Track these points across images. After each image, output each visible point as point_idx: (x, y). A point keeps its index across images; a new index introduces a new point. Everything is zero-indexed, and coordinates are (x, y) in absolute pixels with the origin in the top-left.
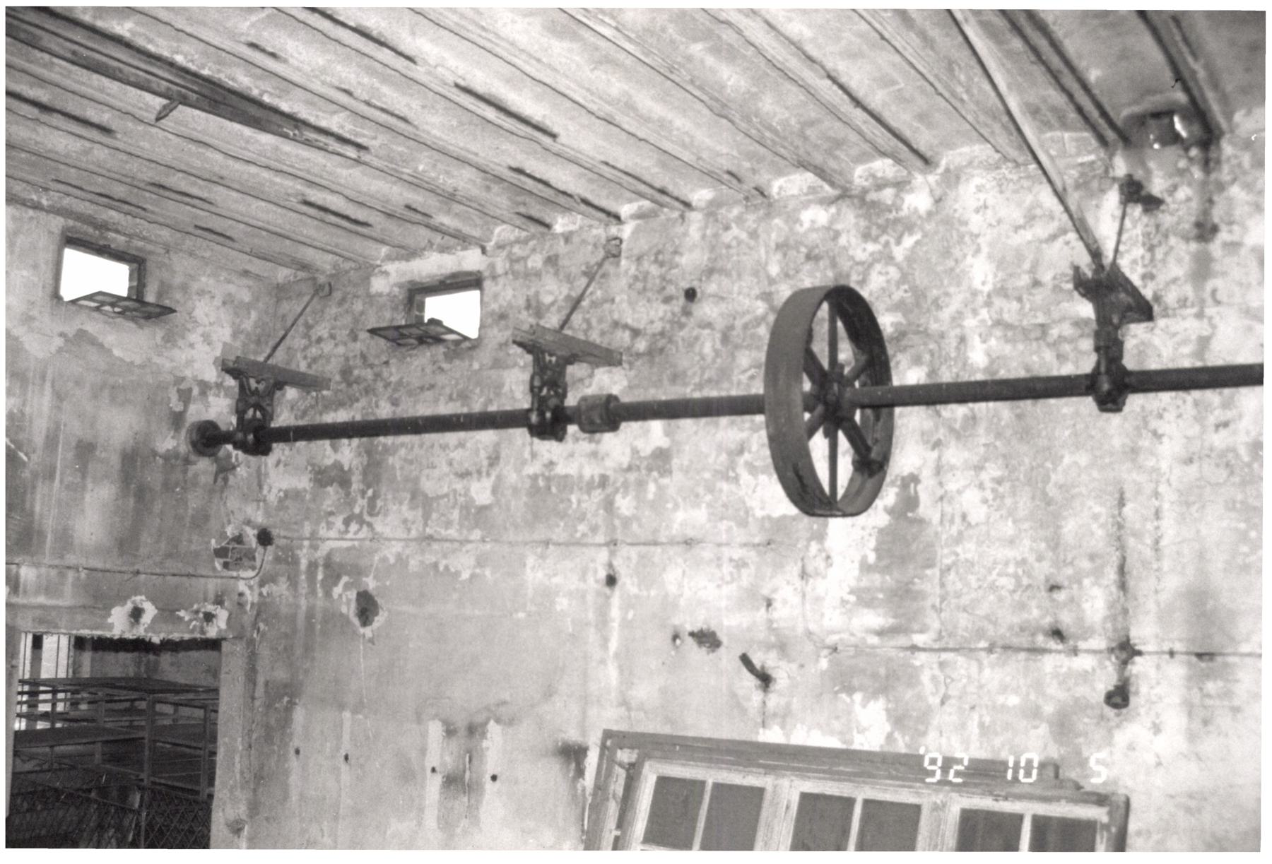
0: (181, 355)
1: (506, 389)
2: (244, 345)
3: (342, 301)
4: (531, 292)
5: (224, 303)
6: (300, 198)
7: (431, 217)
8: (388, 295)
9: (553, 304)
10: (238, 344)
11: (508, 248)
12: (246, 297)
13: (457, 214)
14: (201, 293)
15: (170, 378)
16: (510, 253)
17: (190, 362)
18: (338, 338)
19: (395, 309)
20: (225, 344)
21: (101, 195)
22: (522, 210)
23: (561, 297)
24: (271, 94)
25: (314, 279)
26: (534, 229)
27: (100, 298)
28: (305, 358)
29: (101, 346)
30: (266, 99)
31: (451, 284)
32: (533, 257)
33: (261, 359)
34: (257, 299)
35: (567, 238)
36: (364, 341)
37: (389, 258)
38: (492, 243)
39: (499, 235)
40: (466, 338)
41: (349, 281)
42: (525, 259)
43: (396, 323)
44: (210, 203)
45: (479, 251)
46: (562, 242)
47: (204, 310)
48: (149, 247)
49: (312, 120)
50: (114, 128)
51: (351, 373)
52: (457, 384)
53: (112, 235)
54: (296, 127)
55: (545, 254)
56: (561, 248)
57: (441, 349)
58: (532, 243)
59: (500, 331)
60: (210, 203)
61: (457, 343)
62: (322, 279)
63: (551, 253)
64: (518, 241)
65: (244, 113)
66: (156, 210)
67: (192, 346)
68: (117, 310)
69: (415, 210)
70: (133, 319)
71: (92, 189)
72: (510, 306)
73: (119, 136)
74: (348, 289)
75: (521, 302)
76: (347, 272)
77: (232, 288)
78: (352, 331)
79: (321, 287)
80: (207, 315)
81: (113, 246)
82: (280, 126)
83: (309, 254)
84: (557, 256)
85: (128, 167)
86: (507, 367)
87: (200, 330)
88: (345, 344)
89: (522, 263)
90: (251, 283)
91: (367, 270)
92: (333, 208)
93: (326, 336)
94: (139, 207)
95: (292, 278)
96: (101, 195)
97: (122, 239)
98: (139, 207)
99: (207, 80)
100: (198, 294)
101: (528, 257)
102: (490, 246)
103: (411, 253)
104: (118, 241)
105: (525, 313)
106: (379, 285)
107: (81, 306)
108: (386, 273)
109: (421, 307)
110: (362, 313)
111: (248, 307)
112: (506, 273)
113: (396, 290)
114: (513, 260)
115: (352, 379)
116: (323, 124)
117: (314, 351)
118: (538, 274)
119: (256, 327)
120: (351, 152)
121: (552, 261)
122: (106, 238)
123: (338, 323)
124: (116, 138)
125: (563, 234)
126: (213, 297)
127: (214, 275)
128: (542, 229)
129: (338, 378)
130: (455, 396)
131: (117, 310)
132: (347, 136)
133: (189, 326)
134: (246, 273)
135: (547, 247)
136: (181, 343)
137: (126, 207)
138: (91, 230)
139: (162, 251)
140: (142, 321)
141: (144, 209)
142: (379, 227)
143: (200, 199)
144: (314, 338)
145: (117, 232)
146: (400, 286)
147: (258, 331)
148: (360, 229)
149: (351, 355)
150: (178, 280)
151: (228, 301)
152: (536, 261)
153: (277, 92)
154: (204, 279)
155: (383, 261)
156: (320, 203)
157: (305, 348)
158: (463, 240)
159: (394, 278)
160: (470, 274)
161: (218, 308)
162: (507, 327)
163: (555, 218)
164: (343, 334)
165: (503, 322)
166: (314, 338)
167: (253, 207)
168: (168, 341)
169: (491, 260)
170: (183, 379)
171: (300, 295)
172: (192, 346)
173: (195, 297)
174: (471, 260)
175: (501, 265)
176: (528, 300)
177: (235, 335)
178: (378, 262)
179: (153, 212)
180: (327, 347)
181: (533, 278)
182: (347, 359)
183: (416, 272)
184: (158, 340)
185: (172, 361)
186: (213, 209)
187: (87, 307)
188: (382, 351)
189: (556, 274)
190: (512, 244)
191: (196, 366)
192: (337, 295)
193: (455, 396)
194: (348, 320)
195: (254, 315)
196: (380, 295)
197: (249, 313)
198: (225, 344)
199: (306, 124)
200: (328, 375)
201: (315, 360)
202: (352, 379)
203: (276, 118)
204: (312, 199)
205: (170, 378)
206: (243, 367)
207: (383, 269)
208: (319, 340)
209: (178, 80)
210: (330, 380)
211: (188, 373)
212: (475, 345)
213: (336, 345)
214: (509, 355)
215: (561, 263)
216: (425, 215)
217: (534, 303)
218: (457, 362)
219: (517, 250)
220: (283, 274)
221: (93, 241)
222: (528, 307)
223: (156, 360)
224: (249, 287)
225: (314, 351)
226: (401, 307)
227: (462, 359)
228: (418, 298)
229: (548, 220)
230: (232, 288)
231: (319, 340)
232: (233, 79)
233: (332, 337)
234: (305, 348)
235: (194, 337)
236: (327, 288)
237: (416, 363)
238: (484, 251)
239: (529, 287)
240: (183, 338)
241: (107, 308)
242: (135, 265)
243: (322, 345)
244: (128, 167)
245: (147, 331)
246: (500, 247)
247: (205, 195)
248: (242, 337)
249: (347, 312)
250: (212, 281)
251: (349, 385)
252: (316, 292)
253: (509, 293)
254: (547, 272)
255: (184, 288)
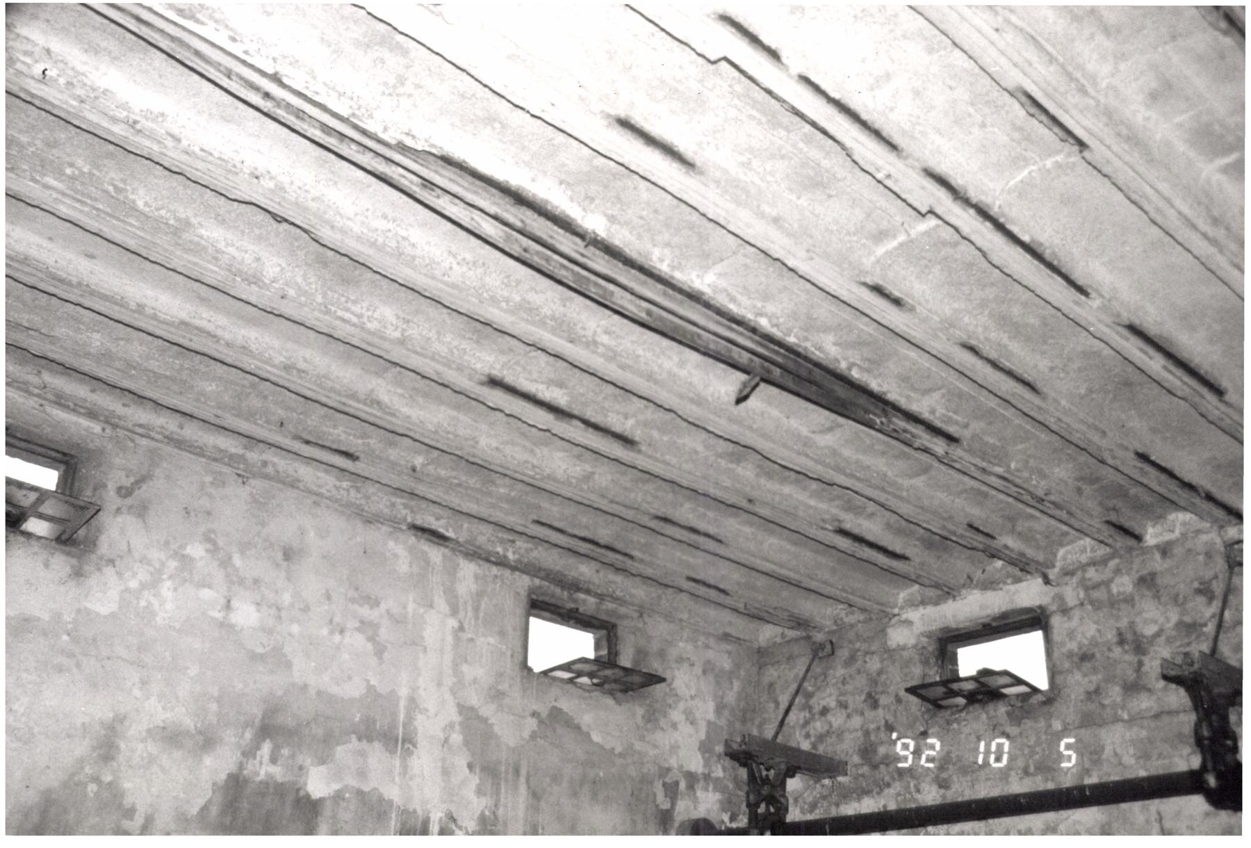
0: (664, 739)
1: (1108, 751)
2: (730, 724)
3: (852, 659)
4: (1124, 623)
5: (704, 672)
6: (836, 524)
7: (993, 537)
8: (915, 646)
9: (1158, 635)
10: (723, 722)
11: (1079, 573)
12: (727, 664)
13: (1019, 533)
14: (680, 660)
15: (653, 769)
16: (1083, 579)
17: (674, 748)
18: (851, 706)
19: (925, 662)
20: (709, 723)
21: (584, 539)
22: (1113, 517)
23: (1171, 625)
24: (860, 367)
25: (809, 638)
26: (1121, 542)
27: (578, 666)
28: (808, 736)
29: (578, 728)
30: (855, 374)
31: (997, 627)
32: (1118, 580)
33: (769, 733)
34: (738, 666)
35: (1165, 550)
36: (886, 707)
37: (912, 604)
38: (1056, 570)
39: (1064, 559)
40: (1035, 690)
41: (857, 635)
42: (1107, 584)
43: (928, 680)
44: (720, 541)
45: (1040, 580)
46: (1158, 556)
47: (683, 680)
48: (623, 610)
49: (903, 403)
50: (637, 439)
51: (875, 751)
52: (1033, 753)
53: (582, 596)
54: (886, 414)
55: (1136, 577)
56: (1157, 563)
57: (1001, 709)
58: (1113, 564)
59: (1085, 675)
60: (720, 541)
61: (1024, 697)
62: (819, 637)
63: (1145, 572)
64: (1093, 563)
65: (829, 393)
66: (647, 558)
67: (674, 726)
68: (595, 681)
69: (977, 530)
70: (611, 693)
71: (576, 532)
72: (1094, 643)
73: (643, 448)
74: (858, 645)
75: (1111, 636)
76: (852, 626)
77: (710, 654)
78: (869, 695)
79: (821, 646)
80: (688, 687)
81: (581, 610)
82: (867, 411)
83: (807, 607)
84: (1153, 575)
85: (632, 496)
86: (1103, 723)
87: (681, 706)
88: (862, 714)
89: (1103, 589)
90: (729, 647)
91: (883, 618)
92: (870, 538)
93: (833, 704)
94: (625, 555)
95: (778, 640)
96: (584, 539)
97: (592, 600)
98: (625, 555)
99: (790, 349)
100: (677, 661)
101: (1111, 580)
102: (1053, 574)
103: (948, 592)
104: (588, 604)
105: (1117, 651)
106: (898, 637)
107: (555, 679)
108: (909, 623)
109: (954, 660)
110: (880, 672)
111: (731, 675)
112: (1082, 604)
113: (925, 640)
114: (1089, 587)
115: (878, 758)
116: (914, 408)
117: (818, 726)
118: (1129, 600)
119: (738, 700)
120: (939, 446)
121: (1147, 582)
122: (575, 601)
123: (849, 687)
124: (639, 451)
125: (1157, 547)
126: (692, 665)
127: (693, 640)
128: (1131, 542)
129: (856, 759)
130: (1032, 769)
131: (595, 681)
132: (938, 424)
133: (670, 701)
134: (726, 637)
135: (1135, 567)
136: (662, 723)
137: (611, 556)
138: (558, 591)
139: (636, 615)
140: (619, 695)
141: (631, 557)
142: (917, 560)
143: (707, 535)
144: (817, 709)
145: (588, 592)
146: (929, 635)
147: (743, 704)
148: (895, 564)
149: (872, 726)
150: (655, 646)
151: (708, 668)
152: (1124, 584)
153: (866, 365)
154: (681, 644)
155: (902, 608)
156: (856, 531)
157: (807, 723)
158: (1023, 566)
159: (919, 627)
160: (1028, 610)
161: (698, 678)
162: (1095, 670)
163: (1145, 527)
164: (857, 701)
165: (1087, 665)
166: (817, 709)
167: (766, 545)
168: (649, 721)
169: (1056, 590)
170: (669, 770)
171: (790, 658)
172: (674, 726)
173: (674, 665)
174: (1029, 593)
175: (1072, 594)
176: (1120, 634)
177: (719, 709)
178: (896, 611)
179: (642, 561)
180: (837, 720)
181: (1123, 606)
182: (867, 733)
183: (949, 615)
184: (639, 720)
185: (655, 746)
186: (721, 550)
187: (562, 680)
188: (916, 719)
189: (1157, 597)
190: (1083, 567)
191: (682, 753)
192: (843, 653)
193: (1032, 769)
194: (861, 682)
195: (736, 685)
196: (904, 648)
197: (731, 683)
198: (709, 723)
199: (896, 408)
200: (843, 757)
201: (821, 738)
202: (878, 758)
203: (863, 400)
204: (847, 526)
205: (653, 769)
206: (754, 748)
207: (904, 617)
208: (825, 711)
209: (760, 350)
210: (846, 763)
211: (673, 762)
212: (1051, 698)
213: (849, 716)
214: (1103, 706)
215: (1159, 581)
216: (987, 535)
217: (1129, 637)
218: (1028, 723)
219: (1091, 573)
220: (767, 634)
221: (559, 603)
222: (1121, 641)
223: (638, 746)
224: (729, 653)
225: (818, 726)
226: (932, 661)
227: (1036, 719)
228: (950, 647)
229: (1137, 531)
230: (710, 654)
231: (825, 711)
232: (820, 349)
233: (843, 705)
234: (807, 723)
235: (676, 715)
236: (829, 647)
237: (967, 730)
238: (1047, 581)
239: (1118, 618)
240: (665, 716)
241: (585, 680)
242: (604, 632)
243: (829, 717)
244: (632, 496)
245: (625, 706)
246: (1068, 573)
247: (712, 530)
248: (726, 713)
249: (859, 672)
250: (690, 647)
251: (875, 767)
252: (815, 655)
253: (1090, 630)
254: (1143, 596)
255: (662, 654)
